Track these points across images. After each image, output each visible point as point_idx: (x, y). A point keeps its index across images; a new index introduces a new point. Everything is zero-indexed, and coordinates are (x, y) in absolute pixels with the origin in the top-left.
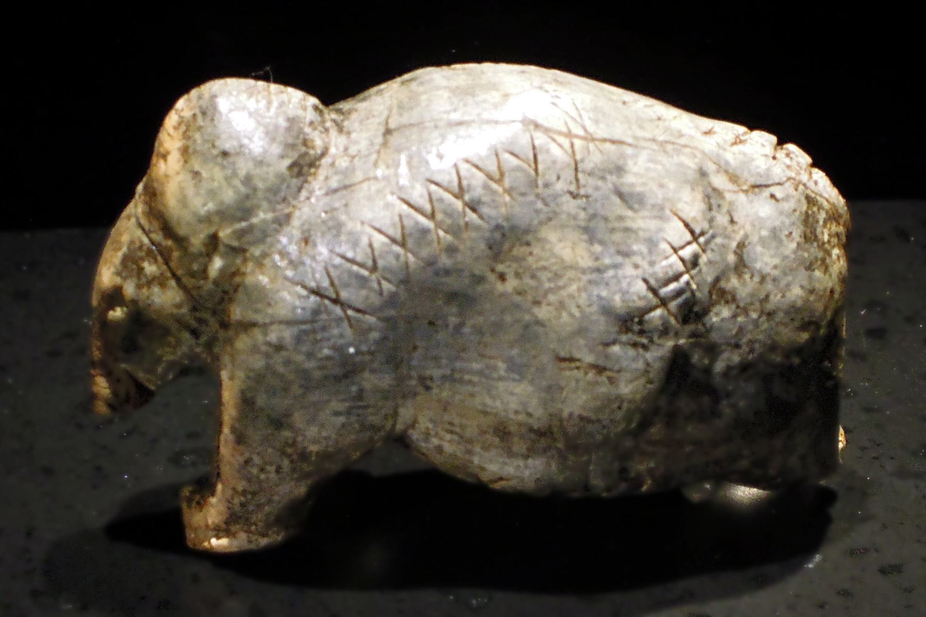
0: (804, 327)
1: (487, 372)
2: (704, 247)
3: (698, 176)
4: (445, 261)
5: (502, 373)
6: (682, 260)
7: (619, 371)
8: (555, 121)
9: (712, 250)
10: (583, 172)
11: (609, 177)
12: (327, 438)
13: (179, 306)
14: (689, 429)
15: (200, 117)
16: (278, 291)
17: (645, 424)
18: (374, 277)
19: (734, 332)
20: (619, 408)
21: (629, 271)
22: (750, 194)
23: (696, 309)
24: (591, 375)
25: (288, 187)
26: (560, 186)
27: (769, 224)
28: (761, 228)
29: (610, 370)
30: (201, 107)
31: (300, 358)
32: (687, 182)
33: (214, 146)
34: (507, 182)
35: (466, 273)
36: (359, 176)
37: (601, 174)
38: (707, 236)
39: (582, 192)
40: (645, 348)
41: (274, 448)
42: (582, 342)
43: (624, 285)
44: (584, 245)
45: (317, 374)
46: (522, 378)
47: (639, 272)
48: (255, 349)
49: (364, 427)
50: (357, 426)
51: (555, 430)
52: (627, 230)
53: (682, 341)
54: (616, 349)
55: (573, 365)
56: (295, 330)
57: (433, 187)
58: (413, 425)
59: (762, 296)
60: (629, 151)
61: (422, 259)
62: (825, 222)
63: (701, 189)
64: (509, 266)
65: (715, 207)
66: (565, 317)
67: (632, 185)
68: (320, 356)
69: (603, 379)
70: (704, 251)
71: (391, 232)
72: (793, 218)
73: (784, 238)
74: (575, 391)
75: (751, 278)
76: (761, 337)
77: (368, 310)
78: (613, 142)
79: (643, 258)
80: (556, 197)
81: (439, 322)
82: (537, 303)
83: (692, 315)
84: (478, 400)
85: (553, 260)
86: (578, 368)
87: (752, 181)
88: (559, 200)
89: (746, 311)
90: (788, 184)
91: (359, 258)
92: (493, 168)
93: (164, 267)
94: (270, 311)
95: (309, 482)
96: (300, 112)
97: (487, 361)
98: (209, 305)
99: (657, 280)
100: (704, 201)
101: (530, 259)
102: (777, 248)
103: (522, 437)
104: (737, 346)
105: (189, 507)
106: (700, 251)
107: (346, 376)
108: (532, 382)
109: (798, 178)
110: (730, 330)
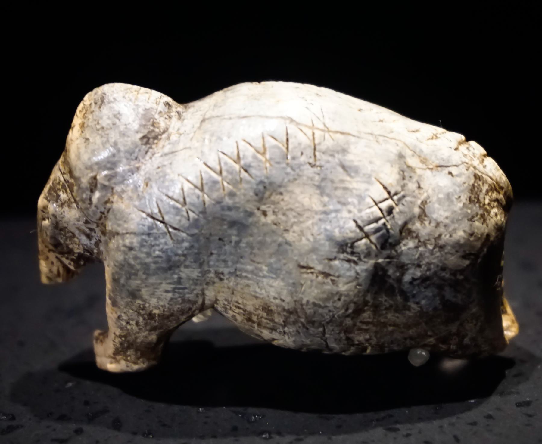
1: (256, 271)
2: (396, 202)
3: (397, 158)
4: (228, 201)
6: (381, 210)
7: (338, 277)
8: (304, 117)
9: (403, 205)
10: (320, 151)
11: (336, 155)
14: (389, 316)
15: (93, 105)
16: (130, 214)
17: (358, 311)
18: (184, 209)
19: (417, 256)
20: (339, 300)
21: (345, 214)
22: (434, 171)
23: (390, 240)
24: (320, 278)
25: (139, 150)
26: (303, 159)
27: (445, 191)
28: (439, 193)
29: (334, 276)
30: (95, 99)
31: (143, 256)
32: (389, 161)
33: (98, 123)
34: (268, 156)
35: (241, 210)
36: (181, 146)
37: (331, 153)
38: (399, 196)
39: (318, 163)
40: (355, 263)
41: (132, 310)
42: (314, 257)
43: (341, 223)
44: (317, 196)
45: (153, 266)
46: (278, 277)
47: (351, 215)
49: (184, 301)
50: (180, 299)
51: (299, 310)
52: (345, 189)
53: (380, 261)
54: (337, 263)
55: (309, 271)
56: (139, 239)
57: (222, 156)
59: (436, 235)
60: (352, 139)
61: (214, 200)
62: (487, 192)
63: (397, 166)
64: (269, 207)
65: (407, 178)
67: (352, 161)
68: (154, 255)
69: (328, 280)
70: (397, 205)
71: (194, 181)
72: (462, 188)
73: (455, 200)
74: (311, 287)
75: (430, 223)
76: (435, 261)
77: (181, 229)
78: (342, 133)
79: (355, 207)
80: (300, 165)
81: (226, 239)
82: (286, 231)
83: (388, 245)
84: (251, 289)
85: (297, 205)
86: (312, 273)
87: (437, 162)
88: (302, 168)
89: (425, 244)
90: (462, 166)
91: (175, 197)
92: (259, 145)
93: (71, 196)
94: (126, 226)
95: (157, 332)
96: (155, 106)
97: (256, 265)
98: (94, 220)
99: (363, 221)
100: (399, 174)
101: (282, 203)
102: (449, 206)
103: (279, 314)
104: (419, 266)
105: (97, 342)
106: (394, 205)
107: (170, 268)
108: (283, 280)
109: (470, 163)
110: (413, 255)
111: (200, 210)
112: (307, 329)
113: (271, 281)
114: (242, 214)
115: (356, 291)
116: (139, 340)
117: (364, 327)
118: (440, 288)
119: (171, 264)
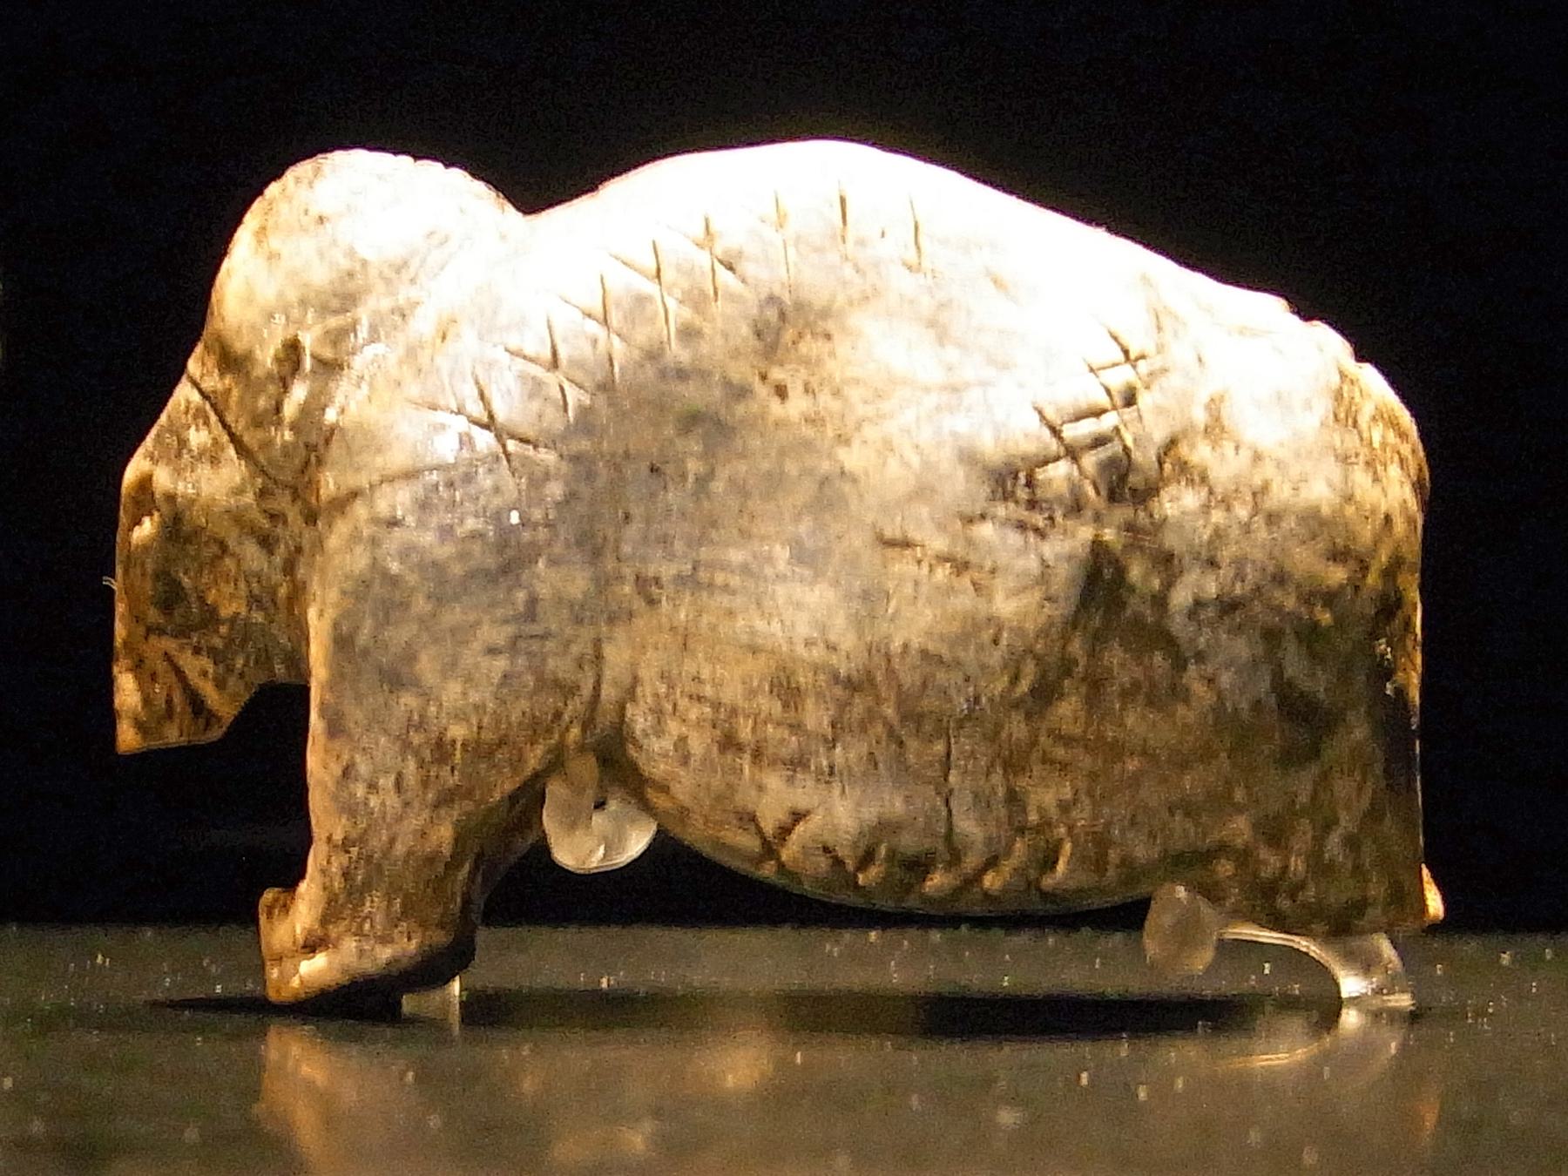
0: (1337, 555)
4: (678, 353)
5: (782, 566)
12: (479, 708)
13: (239, 491)
17: (1045, 693)
24: (942, 573)
31: (428, 538)
40: (1041, 533)
45: (457, 570)
46: (818, 575)
48: (355, 537)
50: (530, 680)
54: (986, 530)
58: (631, 693)
66: (893, 465)
76: (1258, 555)
81: (669, 469)
104: (1213, 563)
108: (836, 583)
111: (599, 377)
112: (901, 744)
113: (799, 591)
114: (717, 393)
115: (1042, 619)
116: (400, 849)
117: (1060, 752)
118: (1271, 636)
119: (510, 553)
